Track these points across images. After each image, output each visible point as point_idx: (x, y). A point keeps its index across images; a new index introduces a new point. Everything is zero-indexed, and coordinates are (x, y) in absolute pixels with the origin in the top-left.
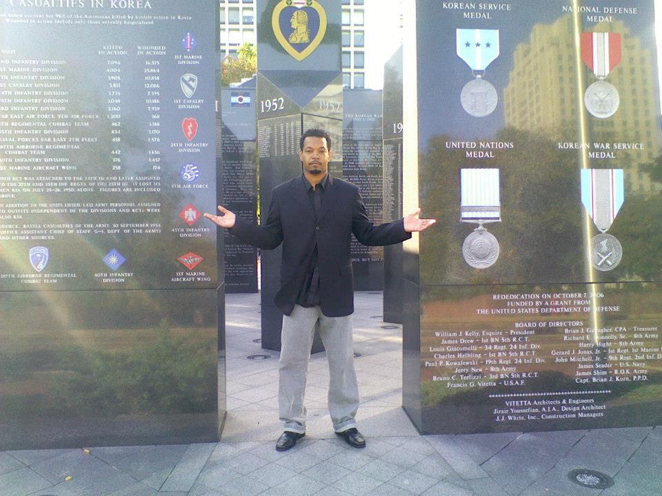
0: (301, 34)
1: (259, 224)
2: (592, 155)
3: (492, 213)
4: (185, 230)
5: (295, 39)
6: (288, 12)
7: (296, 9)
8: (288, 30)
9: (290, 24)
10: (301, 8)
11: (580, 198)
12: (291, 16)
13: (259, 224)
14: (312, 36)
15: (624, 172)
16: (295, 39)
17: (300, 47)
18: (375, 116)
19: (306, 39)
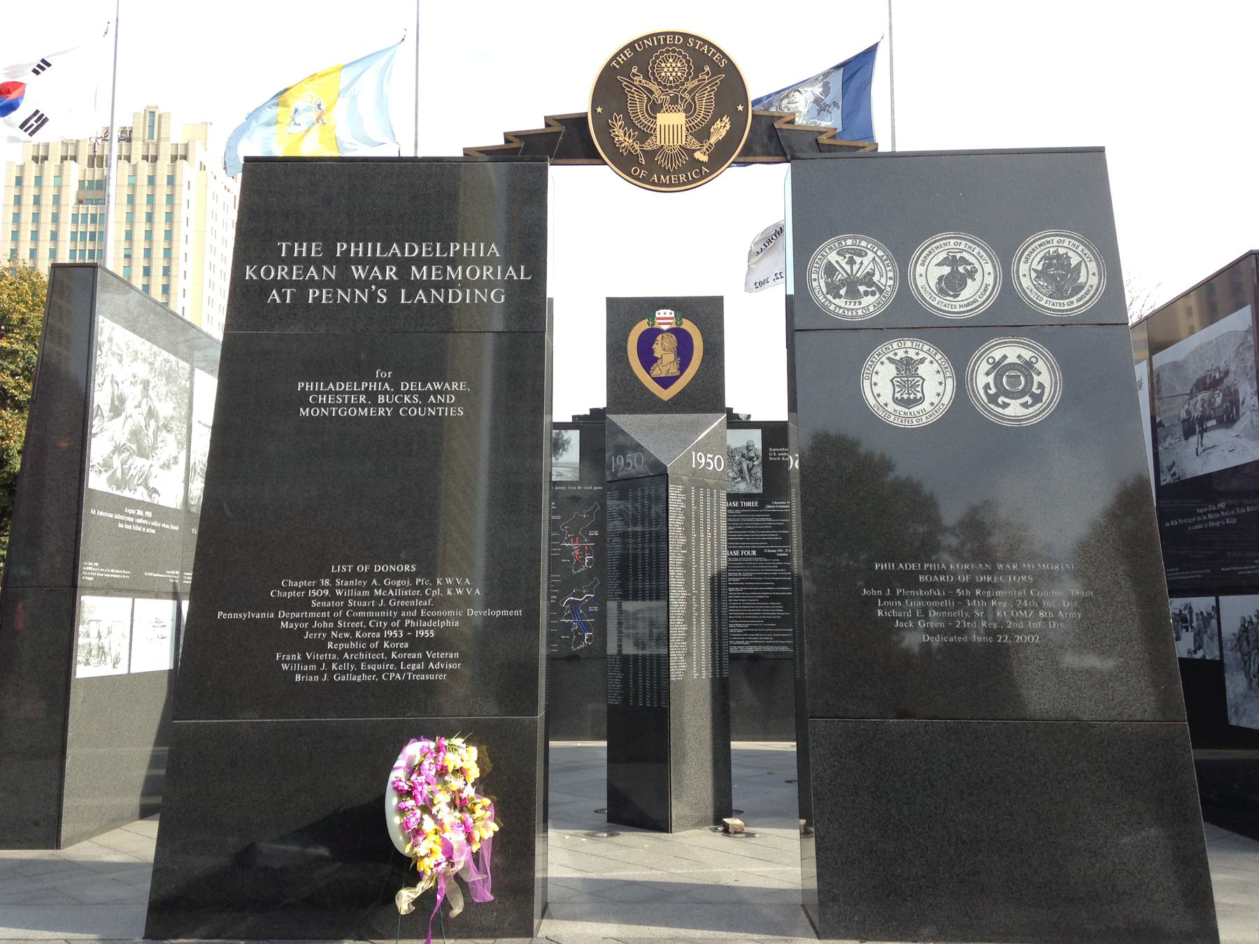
0: (666, 359)
1: (177, 528)
2: (93, 661)
3: (681, 582)
4: (304, 657)
5: (659, 371)
6: (649, 338)
7: (661, 331)
8: (648, 360)
9: (652, 351)
10: (669, 331)
11: (219, 384)
12: (653, 341)
13: (177, 528)
14: (683, 367)
15: (175, 510)
16: (659, 371)
17: (665, 382)
18: (939, 657)
19: (674, 371)
